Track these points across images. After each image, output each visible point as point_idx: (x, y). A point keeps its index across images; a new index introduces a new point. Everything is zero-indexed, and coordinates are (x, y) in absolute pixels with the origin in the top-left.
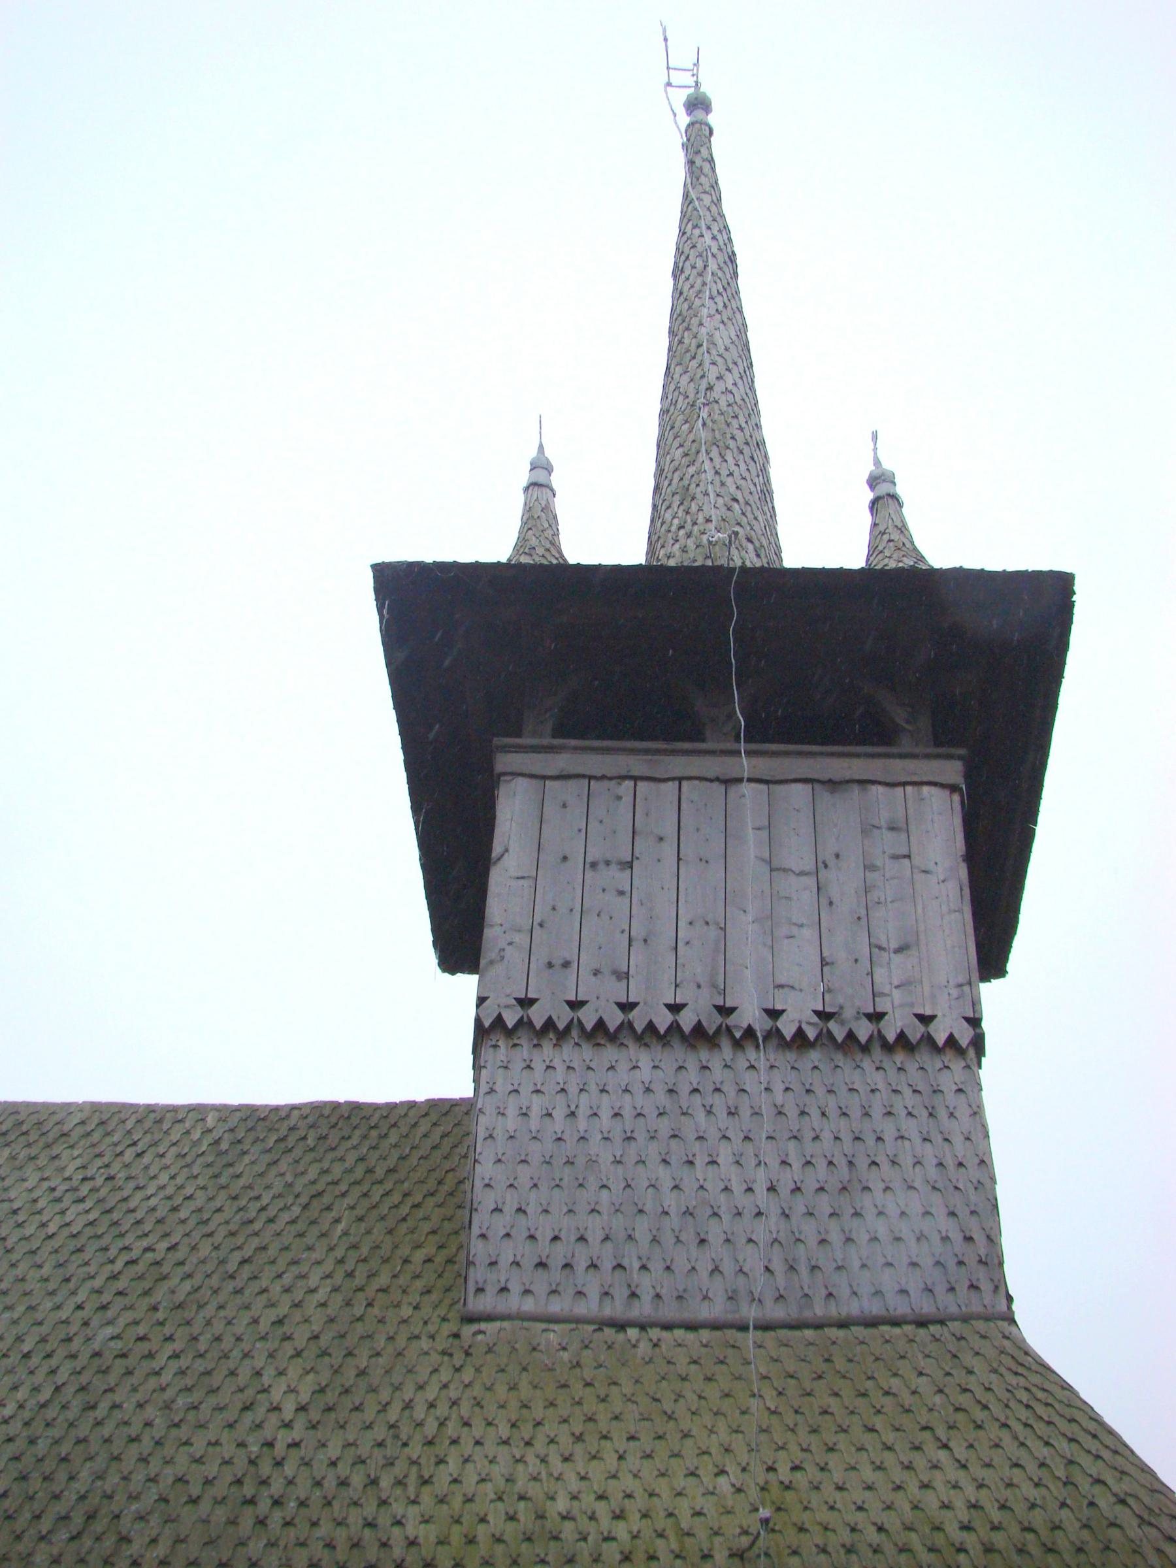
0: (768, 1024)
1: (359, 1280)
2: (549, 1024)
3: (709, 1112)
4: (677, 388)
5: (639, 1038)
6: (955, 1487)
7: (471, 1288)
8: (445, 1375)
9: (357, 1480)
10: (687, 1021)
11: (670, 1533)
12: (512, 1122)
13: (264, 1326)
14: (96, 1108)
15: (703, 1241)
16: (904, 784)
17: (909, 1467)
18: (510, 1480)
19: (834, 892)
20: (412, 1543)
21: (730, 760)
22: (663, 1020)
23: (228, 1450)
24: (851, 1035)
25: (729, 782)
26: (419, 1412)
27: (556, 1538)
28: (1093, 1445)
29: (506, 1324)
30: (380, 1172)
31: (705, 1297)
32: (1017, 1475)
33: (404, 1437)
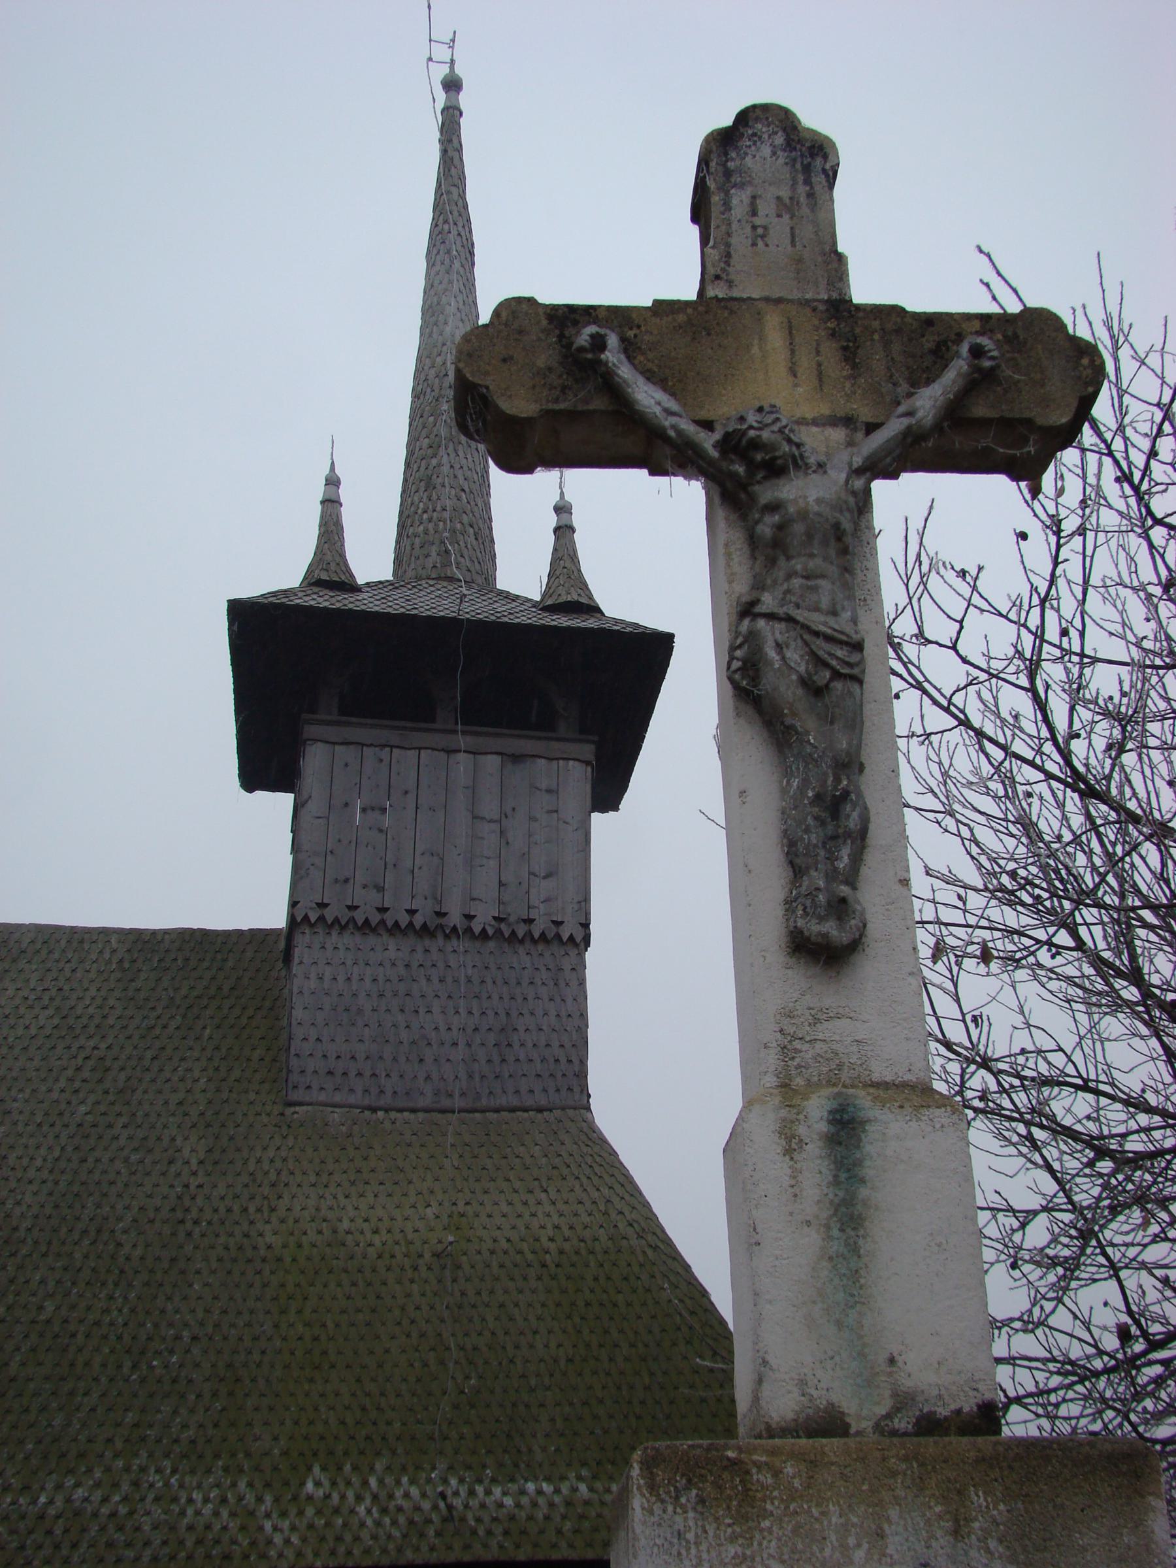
2: (337, 920)
3: (428, 980)
4: (426, 380)
6: (548, 1215)
7: (290, 1085)
8: (278, 1141)
9: (236, 1208)
10: (418, 921)
11: (403, 1243)
12: (313, 984)
13: (172, 1107)
14: (39, 928)
15: (421, 1060)
16: (557, 759)
17: (525, 1204)
18: (318, 1209)
20: (269, 1247)
22: (404, 920)
25: (450, 752)
26: (266, 1166)
27: (344, 1245)
29: (310, 1108)
31: (422, 1093)
32: (580, 1209)
33: (259, 1181)
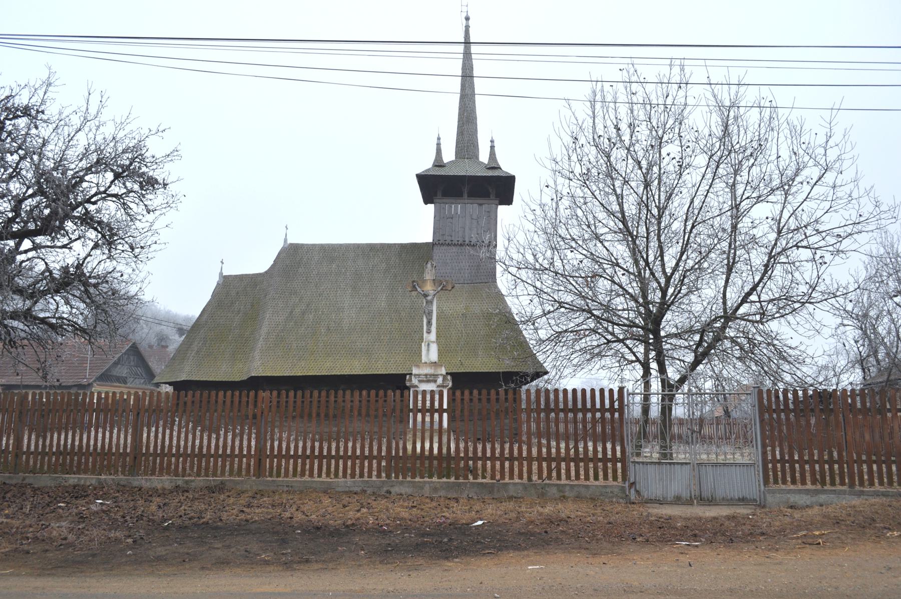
14: (381, 244)
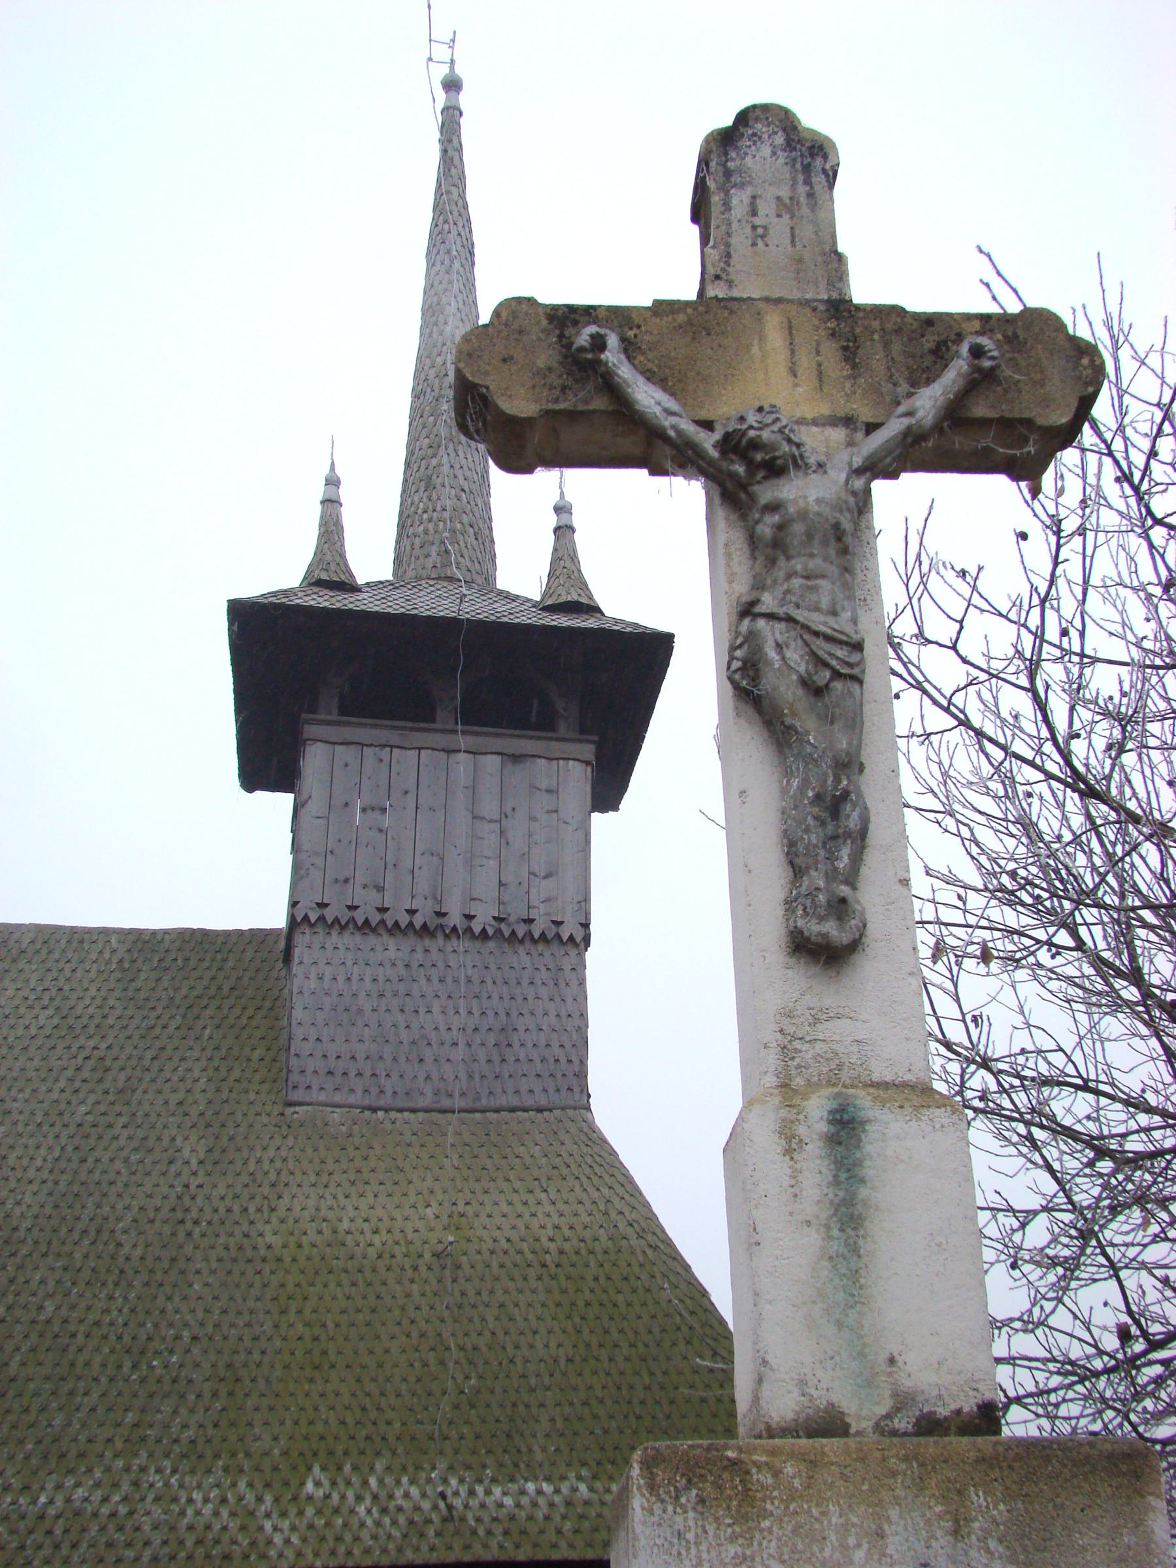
0: (465, 923)
1: (223, 1073)
2: (337, 920)
5: (390, 932)
7: (290, 1085)
8: (278, 1141)
9: (236, 1208)
10: (418, 921)
12: (313, 984)
13: (172, 1106)
14: (39, 929)
17: (525, 1204)
19: (510, 835)
20: (269, 1247)
21: (453, 737)
22: (404, 920)
23: (165, 1190)
24: (513, 933)
25: (450, 752)
26: (266, 1165)
28: (621, 1191)
30: (226, 989)
